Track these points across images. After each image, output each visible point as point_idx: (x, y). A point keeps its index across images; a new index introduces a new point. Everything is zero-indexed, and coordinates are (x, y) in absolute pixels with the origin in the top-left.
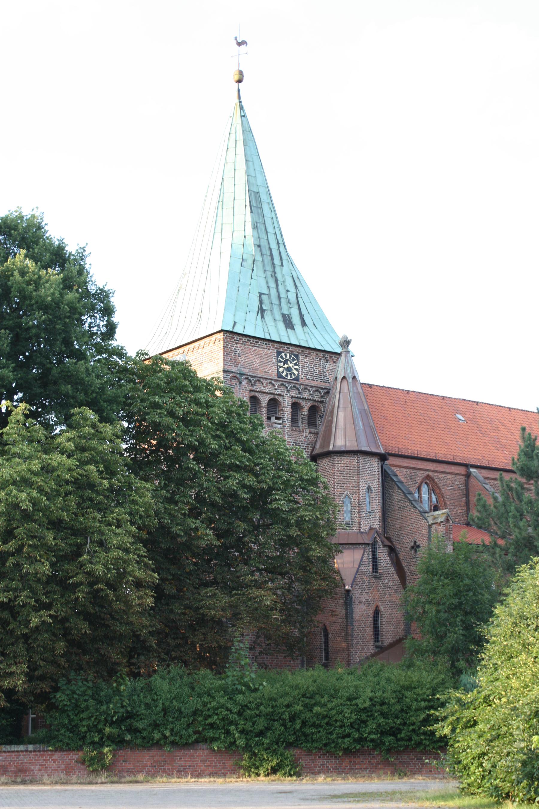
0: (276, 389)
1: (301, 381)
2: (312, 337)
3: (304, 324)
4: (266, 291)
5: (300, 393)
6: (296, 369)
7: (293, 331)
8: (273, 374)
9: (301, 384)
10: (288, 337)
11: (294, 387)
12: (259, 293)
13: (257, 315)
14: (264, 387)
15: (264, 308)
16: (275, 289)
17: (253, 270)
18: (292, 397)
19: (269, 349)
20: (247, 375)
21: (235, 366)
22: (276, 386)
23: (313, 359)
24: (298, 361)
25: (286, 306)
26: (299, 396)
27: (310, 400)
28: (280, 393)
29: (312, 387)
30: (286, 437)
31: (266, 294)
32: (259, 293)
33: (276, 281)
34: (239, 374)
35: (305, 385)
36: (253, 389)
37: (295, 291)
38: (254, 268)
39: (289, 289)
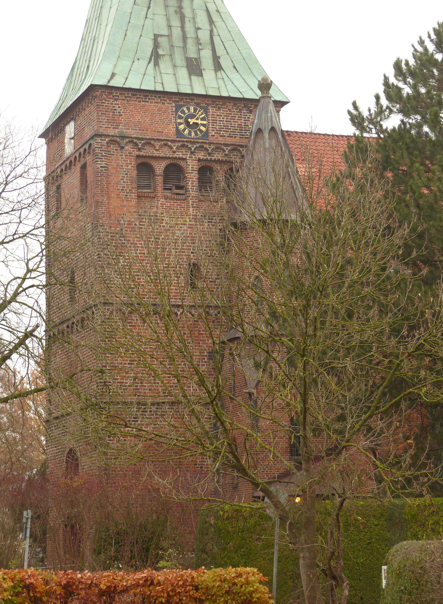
0: (174, 152)
1: (211, 139)
2: (228, 82)
3: (218, 67)
4: (165, 32)
5: (209, 154)
6: (204, 125)
7: (200, 78)
8: (170, 132)
9: (210, 144)
10: (191, 85)
11: (200, 147)
12: (155, 35)
13: (149, 62)
14: (157, 150)
15: (160, 52)
16: (179, 29)
17: (149, 8)
18: (199, 160)
19: (164, 103)
20: (132, 138)
21: (114, 128)
22: (175, 148)
23: (230, 110)
24: (207, 115)
25: (194, 48)
26: (209, 158)
27: (226, 161)
28: (181, 156)
29: (227, 145)
30: (191, 209)
31: (165, 36)
32: (155, 35)
33: (182, 18)
34: (119, 137)
35: (217, 144)
36: (141, 154)
37: (209, 28)
38: (151, 5)
39: (200, 26)
